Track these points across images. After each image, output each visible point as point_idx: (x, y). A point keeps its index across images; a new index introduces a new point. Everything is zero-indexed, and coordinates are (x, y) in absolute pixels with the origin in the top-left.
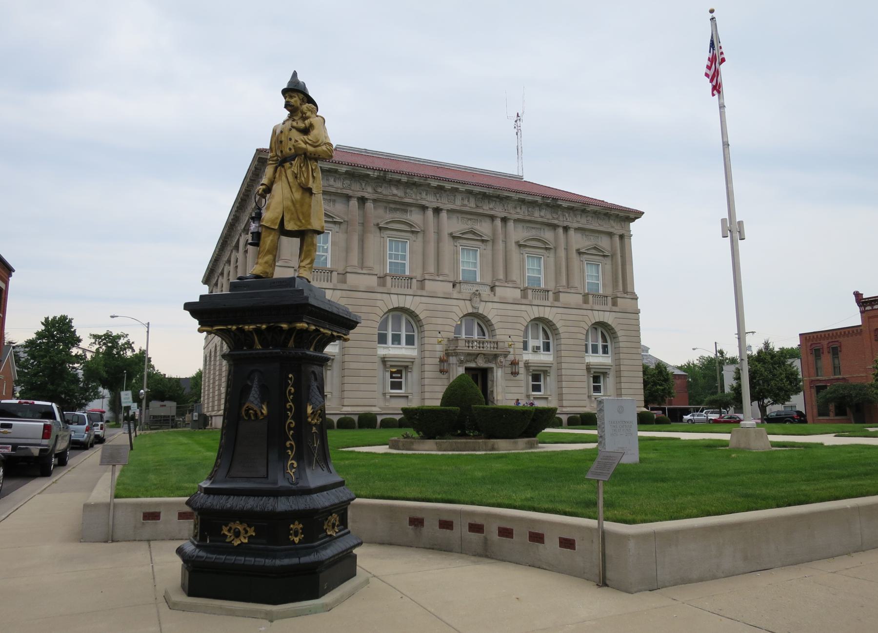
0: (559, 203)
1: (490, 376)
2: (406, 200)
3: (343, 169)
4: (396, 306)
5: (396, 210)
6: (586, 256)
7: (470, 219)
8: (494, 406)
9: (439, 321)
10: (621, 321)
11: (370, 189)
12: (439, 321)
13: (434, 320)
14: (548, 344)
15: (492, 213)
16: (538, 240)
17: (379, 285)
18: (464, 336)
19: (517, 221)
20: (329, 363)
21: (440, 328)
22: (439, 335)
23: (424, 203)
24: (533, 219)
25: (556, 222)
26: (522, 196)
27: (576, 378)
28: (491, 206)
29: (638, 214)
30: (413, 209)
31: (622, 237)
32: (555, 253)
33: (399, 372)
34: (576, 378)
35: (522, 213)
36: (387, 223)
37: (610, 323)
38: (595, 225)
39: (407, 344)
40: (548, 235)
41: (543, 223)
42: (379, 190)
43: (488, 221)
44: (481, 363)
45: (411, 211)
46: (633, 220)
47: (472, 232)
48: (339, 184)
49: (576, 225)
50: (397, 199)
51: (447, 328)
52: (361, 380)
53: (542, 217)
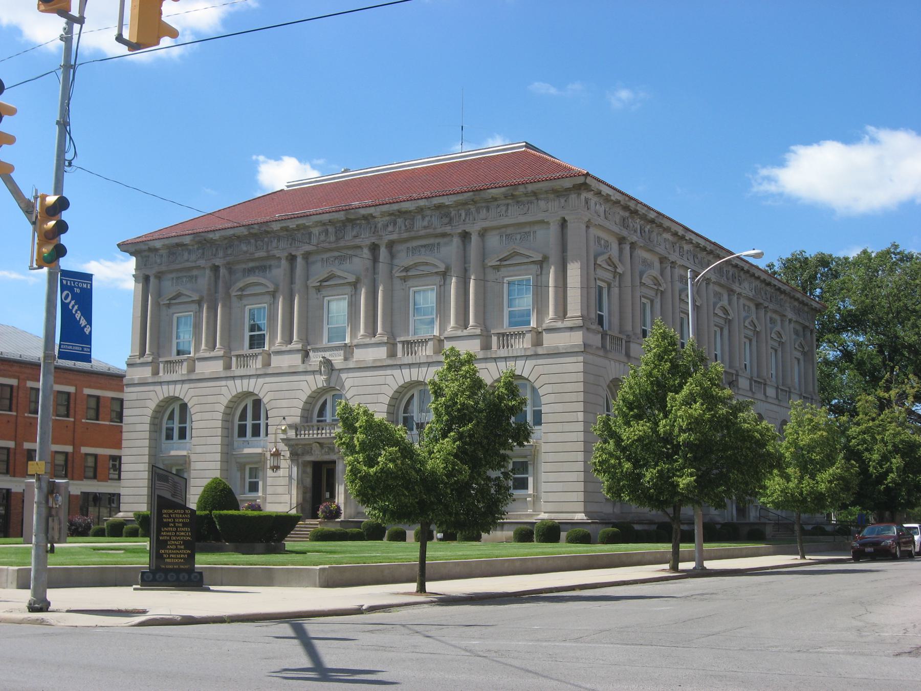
9: (284, 403)
11: (221, 254)
25: (448, 229)
27: (559, 487)
45: (270, 266)
47: (516, 254)
48: (193, 257)
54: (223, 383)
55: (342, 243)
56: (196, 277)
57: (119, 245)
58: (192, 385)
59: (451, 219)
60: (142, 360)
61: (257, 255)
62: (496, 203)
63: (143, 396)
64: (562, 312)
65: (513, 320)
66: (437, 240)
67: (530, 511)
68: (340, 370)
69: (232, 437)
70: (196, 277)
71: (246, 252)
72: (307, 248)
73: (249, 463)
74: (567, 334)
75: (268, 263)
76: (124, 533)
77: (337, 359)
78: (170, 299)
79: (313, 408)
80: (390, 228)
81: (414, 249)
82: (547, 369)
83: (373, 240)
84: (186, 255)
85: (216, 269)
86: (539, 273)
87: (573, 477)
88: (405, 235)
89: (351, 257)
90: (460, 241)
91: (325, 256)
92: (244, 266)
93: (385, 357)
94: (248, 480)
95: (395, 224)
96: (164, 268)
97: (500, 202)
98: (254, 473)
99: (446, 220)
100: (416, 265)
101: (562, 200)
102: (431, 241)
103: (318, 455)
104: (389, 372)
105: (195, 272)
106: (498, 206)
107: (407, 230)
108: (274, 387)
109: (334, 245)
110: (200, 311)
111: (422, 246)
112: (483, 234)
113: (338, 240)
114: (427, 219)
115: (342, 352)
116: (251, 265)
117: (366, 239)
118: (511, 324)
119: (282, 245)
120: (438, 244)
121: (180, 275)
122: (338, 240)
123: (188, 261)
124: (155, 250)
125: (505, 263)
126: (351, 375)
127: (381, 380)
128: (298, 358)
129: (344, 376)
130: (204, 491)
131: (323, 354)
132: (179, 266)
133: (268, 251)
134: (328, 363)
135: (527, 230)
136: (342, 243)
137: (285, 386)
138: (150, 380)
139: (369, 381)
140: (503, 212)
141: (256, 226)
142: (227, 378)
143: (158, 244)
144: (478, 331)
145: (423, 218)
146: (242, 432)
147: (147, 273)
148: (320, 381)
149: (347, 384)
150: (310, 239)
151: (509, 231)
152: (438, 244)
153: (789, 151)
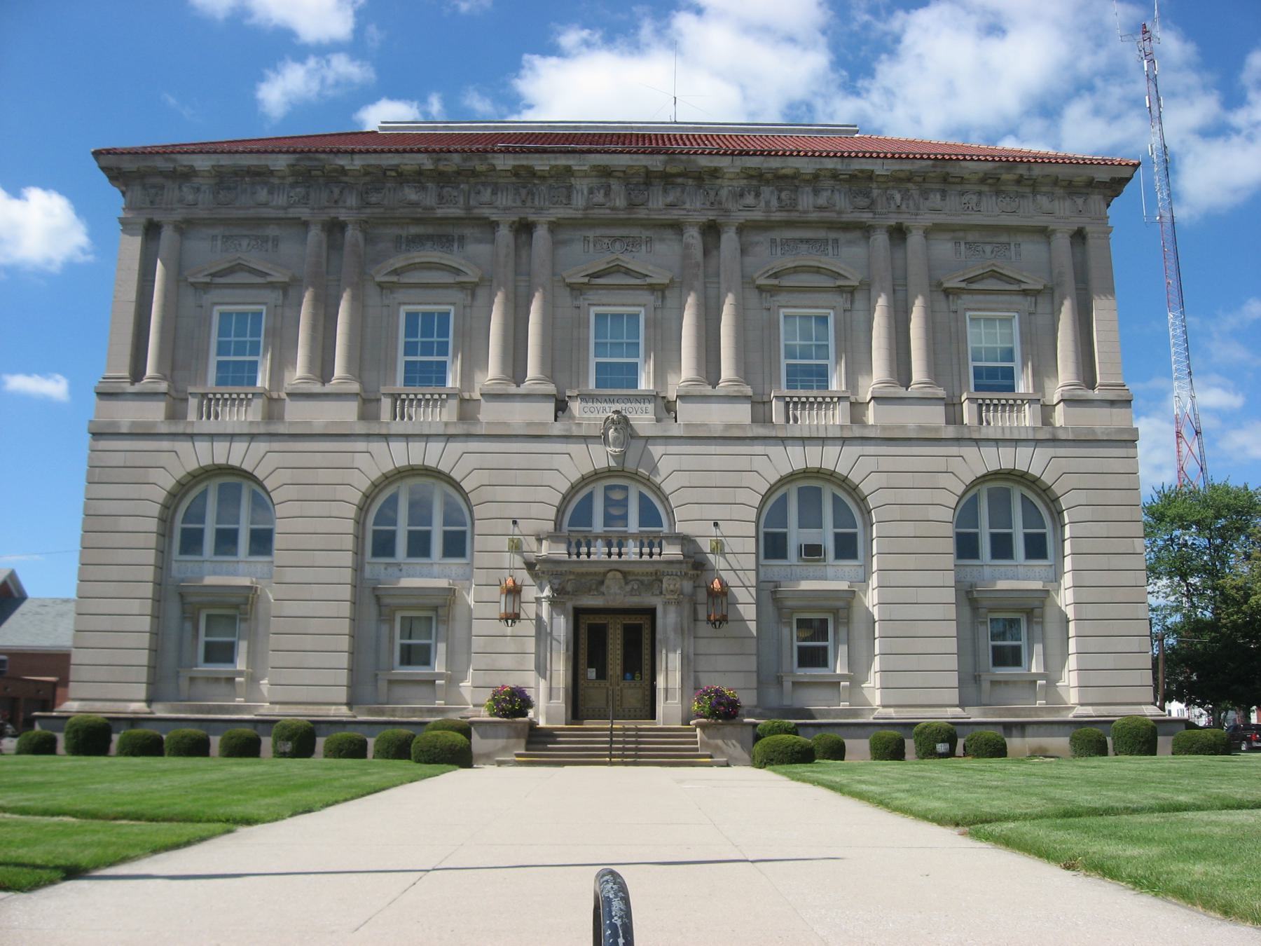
0: (186, 160)
4: (981, 471)
5: (417, 241)
9: (515, 494)
11: (352, 200)
13: (500, 493)
15: (674, 214)
17: (363, 416)
21: (515, 511)
24: (794, 216)
25: (866, 217)
30: (467, 232)
33: (1014, 623)
35: (763, 206)
38: (992, 211)
39: (253, 552)
41: (831, 226)
42: (374, 198)
43: (669, 234)
45: (462, 239)
47: (995, 275)
48: (280, 200)
49: (928, 219)
51: (535, 510)
52: (308, 642)
54: (361, 445)
55: (641, 214)
57: (97, 154)
58: (276, 446)
59: (873, 202)
60: (137, 388)
61: (440, 212)
62: (959, 188)
63: (543, 461)
64: (322, 366)
65: (980, 382)
66: (832, 235)
67: (1040, 703)
68: (648, 439)
69: (363, 554)
70: (276, 241)
71: (415, 204)
72: (559, 212)
73: (402, 608)
74: (1106, 411)
75: (456, 232)
76: (114, 746)
77: (643, 418)
78: (213, 275)
80: (750, 199)
81: (785, 243)
82: (1075, 465)
83: (711, 215)
84: (487, 195)
85: (335, 228)
86: (280, 302)
87: (1134, 644)
88: (778, 216)
89: (649, 240)
90: (323, 236)
92: (396, 231)
93: (748, 420)
94: (398, 641)
95: (757, 195)
96: (201, 213)
97: (968, 187)
98: (817, 629)
100: (796, 270)
101: (1080, 201)
102: (821, 234)
103: (615, 595)
104: (758, 449)
105: (272, 231)
106: (962, 194)
109: (623, 215)
111: (802, 241)
112: (928, 232)
114: (825, 194)
115: (651, 407)
116: (415, 230)
118: (221, 382)
119: (504, 200)
120: (836, 241)
122: (632, 205)
123: (266, 205)
124: (188, 175)
125: (974, 286)
127: (742, 463)
128: (546, 410)
129: (656, 450)
131: (617, 406)
132: (241, 214)
134: (623, 423)
136: (641, 214)
137: (516, 461)
138: (164, 429)
139: (715, 463)
140: (973, 204)
142: (368, 436)
143: (202, 163)
144: (163, 387)
145: (816, 192)
146: (192, 542)
147: (156, 218)
148: (601, 456)
149: (665, 466)
150: (569, 197)
151: (971, 237)
152: (836, 241)
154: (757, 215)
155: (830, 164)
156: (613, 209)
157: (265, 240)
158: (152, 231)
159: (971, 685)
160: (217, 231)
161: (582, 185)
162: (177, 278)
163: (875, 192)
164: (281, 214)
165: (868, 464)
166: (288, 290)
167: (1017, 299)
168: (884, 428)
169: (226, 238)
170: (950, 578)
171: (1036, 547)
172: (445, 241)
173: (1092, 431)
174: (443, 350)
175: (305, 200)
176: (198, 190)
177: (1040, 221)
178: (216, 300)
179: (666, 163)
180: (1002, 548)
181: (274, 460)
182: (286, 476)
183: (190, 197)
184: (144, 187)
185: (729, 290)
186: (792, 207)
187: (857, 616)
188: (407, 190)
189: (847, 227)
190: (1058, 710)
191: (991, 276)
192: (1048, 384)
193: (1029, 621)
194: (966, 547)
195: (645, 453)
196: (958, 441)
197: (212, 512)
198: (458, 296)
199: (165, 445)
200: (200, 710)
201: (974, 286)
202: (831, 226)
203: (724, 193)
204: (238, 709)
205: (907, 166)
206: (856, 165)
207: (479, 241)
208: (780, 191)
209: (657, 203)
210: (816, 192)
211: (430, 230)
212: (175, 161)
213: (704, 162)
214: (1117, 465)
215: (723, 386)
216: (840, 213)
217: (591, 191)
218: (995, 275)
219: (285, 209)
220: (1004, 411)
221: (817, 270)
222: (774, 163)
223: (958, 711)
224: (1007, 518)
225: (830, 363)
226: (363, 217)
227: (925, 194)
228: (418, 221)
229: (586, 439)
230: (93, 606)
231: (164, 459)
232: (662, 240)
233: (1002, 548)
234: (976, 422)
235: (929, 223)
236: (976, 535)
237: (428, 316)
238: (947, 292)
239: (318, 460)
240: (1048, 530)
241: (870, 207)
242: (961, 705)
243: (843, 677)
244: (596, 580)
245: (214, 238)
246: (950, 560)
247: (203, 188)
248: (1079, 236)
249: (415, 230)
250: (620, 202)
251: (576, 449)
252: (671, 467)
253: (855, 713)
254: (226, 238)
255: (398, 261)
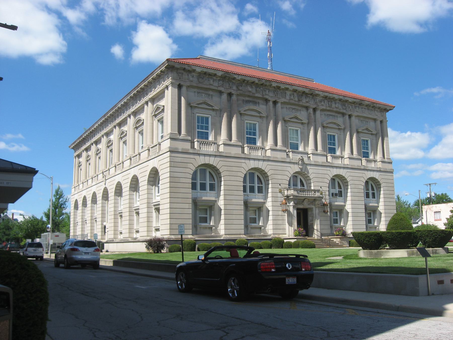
1: (309, 213)
2: (257, 95)
3: (220, 74)
5: (248, 102)
6: (361, 134)
7: (294, 109)
8: (377, 231)
9: (279, 177)
10: (383, 177)
11: (235, 88)
12: (279, 177)
13: (276, 177)
14: (341, 191)
15: (307, 105)
16: (335, 123)
18: (300, 187)
19: (322, 110)
20: (262, 209)
21: (280, 182)
22: (280, 187)
23: (267, 97)
25: (344, 111)
26: (326, 94)
27: (235, 212)
28: (307, 100)
29: (392, 108)
31: (381, 122)
32: (344, 132)
34: (235, 212)
35: (324, 105)
36: (245, 111)
37: (377, 178)
38: (367, 114)
40: (340, 120)
41: (337, 112)
42: (240, 88)
43: (304, 109)
44: (305, 205)
46: (388, 111)
47: (296, 118)
48: (216, 84)
50: (251, 94)
52: (234, 217)
53: (336, 108)
54: (243, 161)
56: (212, 95)
58: (222, 159)
71: (250, 92)
72: (283, 100)
75: (257, 101)
79: (263, 177)
80: (323, 103)
84: (267, 92)
85: (230, 95)
88: (328, 108)
91: (288, 106)
92: (243, 98)
99: (344, 108)
105: (211, 93)
106: (362, 108)
107: (329, 107)
108: (274, 167)
109: (297, 103)
110: (221, 117)
113: (299, 101)
116: (247, 99)
117: (312, 105)
121: (201, 91)
122: (299, 101)
125: (200, 106)
126: (312, 167)
127: (325, 172)
129: (309, 167)
130: (389, 223)
131: (302, 155)
133: (263, 95)
135: (367, 120)
136: (301, 103)
137: (280, 168)
139: (321, 172)
141: (264, 81)
148: (297, 168)
149: (310, 171)
153: (63, 54)
154: (324, 108)
155: (341, 97)
156: (295, 101)
157: (209, 95)
158: (180, 87)
159: (195, 229)
160: (195, 90)
161: (288, 93)
162: (189, 105)
163: (346, 105)
164: (216, 88)
165: (348, 174)
166: (220, 112)
167: (370, 135)
168: (351, 165)
169: (198, 93)
170: (363, 203)
171: (212, 188)
172: (255, 103)
173: (386, 169)
174: (207, 128)
175: (222, 86)
176: (193, 77)
177: (375, 117)
178: (198, 112)
179: (309, 91)
180: (203, 187)
181: (222, 163)
182: (225, 168)
183: (191, 79)
184: (177, 73)
185: (319, 127)
186: (330, 106)
187: (264, 209)
188: (248, 87)
189: (339, 113)
190: (217, 237)
191: (204, 104)
192: (265, 143)
193: (373, 213)
194: (194, 187)
195: (306, 168)
196: (194, 154)
197: (207, 177)
198: (259, 119)
199: (192, 156)
200: (207, 237)
201: (200, 106)
202: (337, 112)
203: (317, 100)
204: (212, 237)
205: (355, 100)
206: (346, 99)
207: (263, 104)
208: (329, 102)
209: (304, 101)
210: (335, 103)
211: (251, 99)
212: (191, 67)
213: (317, 92)
214: (390, 177)
215: (319, 152)
216: (340, 109)
217: (290, 95)
218: (205, 103)
219: (217, 87)
220: (207, 145)
221: (335, 123)
222: (331, 95)
223: (244, 236)
224: (256, 181)
225: (299, 142)
226: (238, 93)
227: (355, 107)
228: (249, 96)
229: (294, 163)
230: (175, 206)
231: (192, 161)
232: (303, 111)
233: (203, 187)
234: (199, 149)
235: (189, 85)
236: (254, 186)
237: (202, 118)
238: (191, 107)
239: (233, 164)
240: (216, 182)
241: (346, 109)
242: (192, 235)
243: (263, 226)
244: (303, 200)
245: (195, 92)
246: (363, 198)
247: (194, 76)
248: (381, 122)
249: (247, 99)
250: (296, 99)
251: (292, 165)
252: (312, 171)
253: (217, 237)
254: (198, 93)
255: (246, 108)
